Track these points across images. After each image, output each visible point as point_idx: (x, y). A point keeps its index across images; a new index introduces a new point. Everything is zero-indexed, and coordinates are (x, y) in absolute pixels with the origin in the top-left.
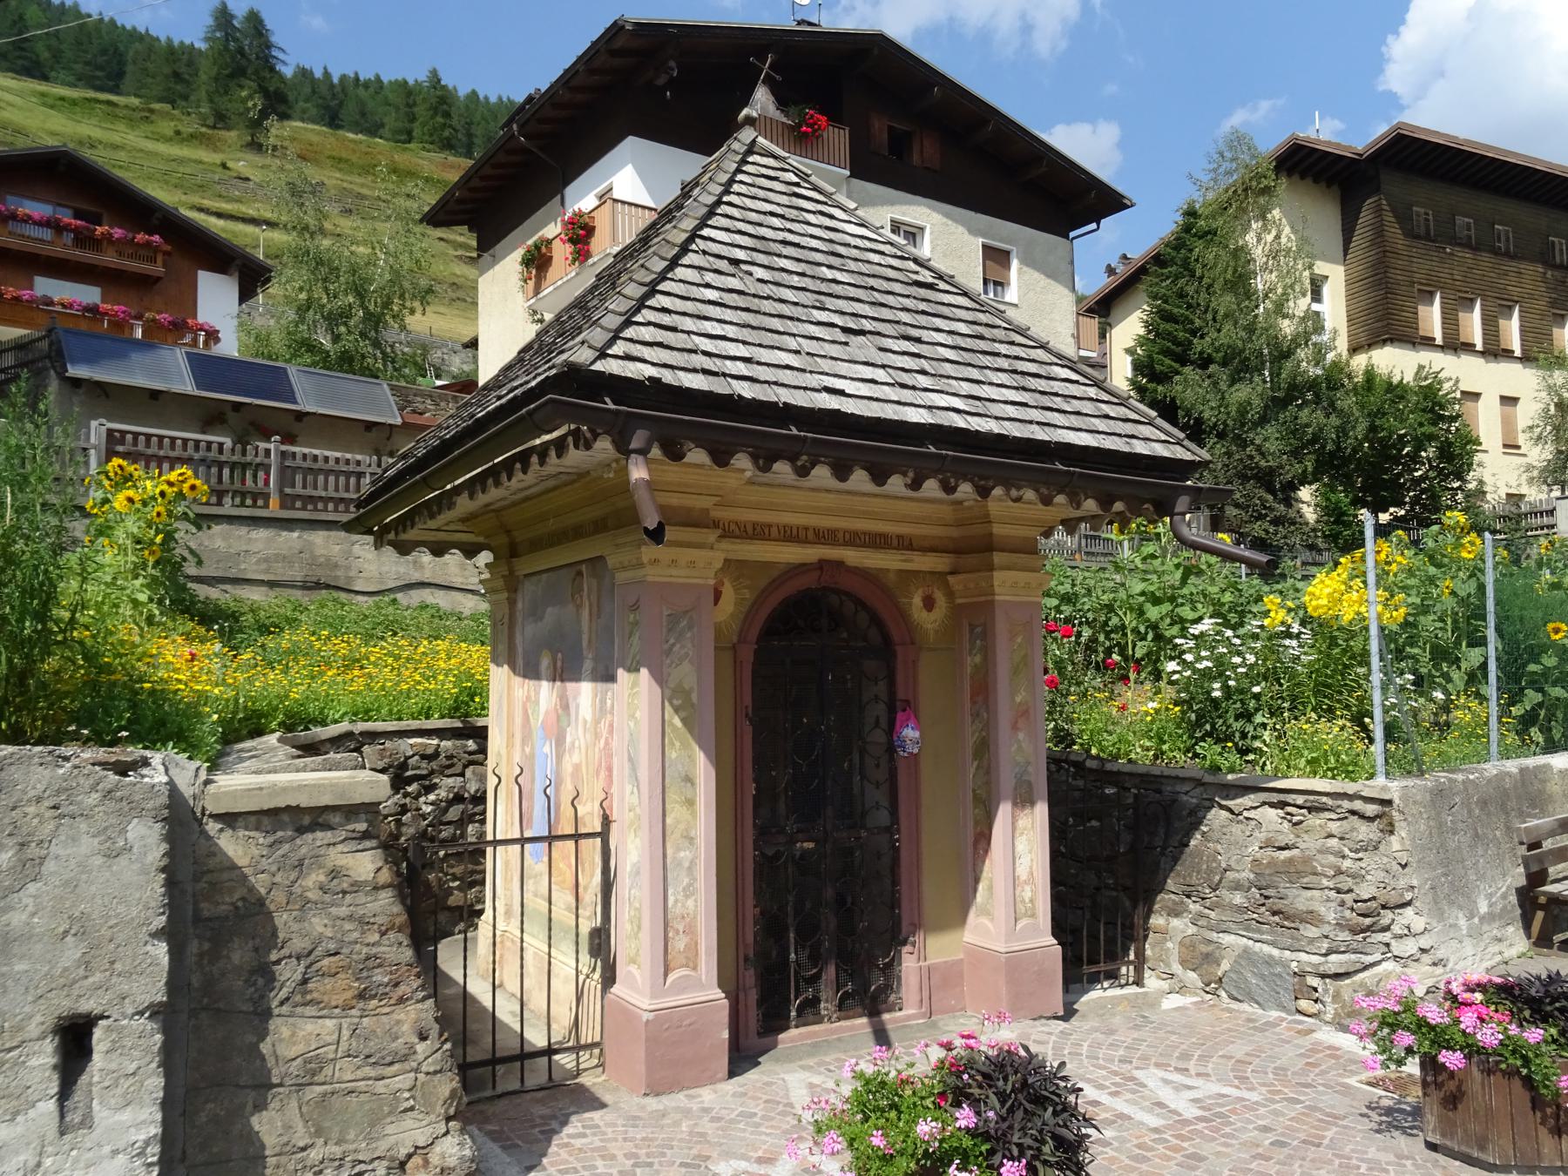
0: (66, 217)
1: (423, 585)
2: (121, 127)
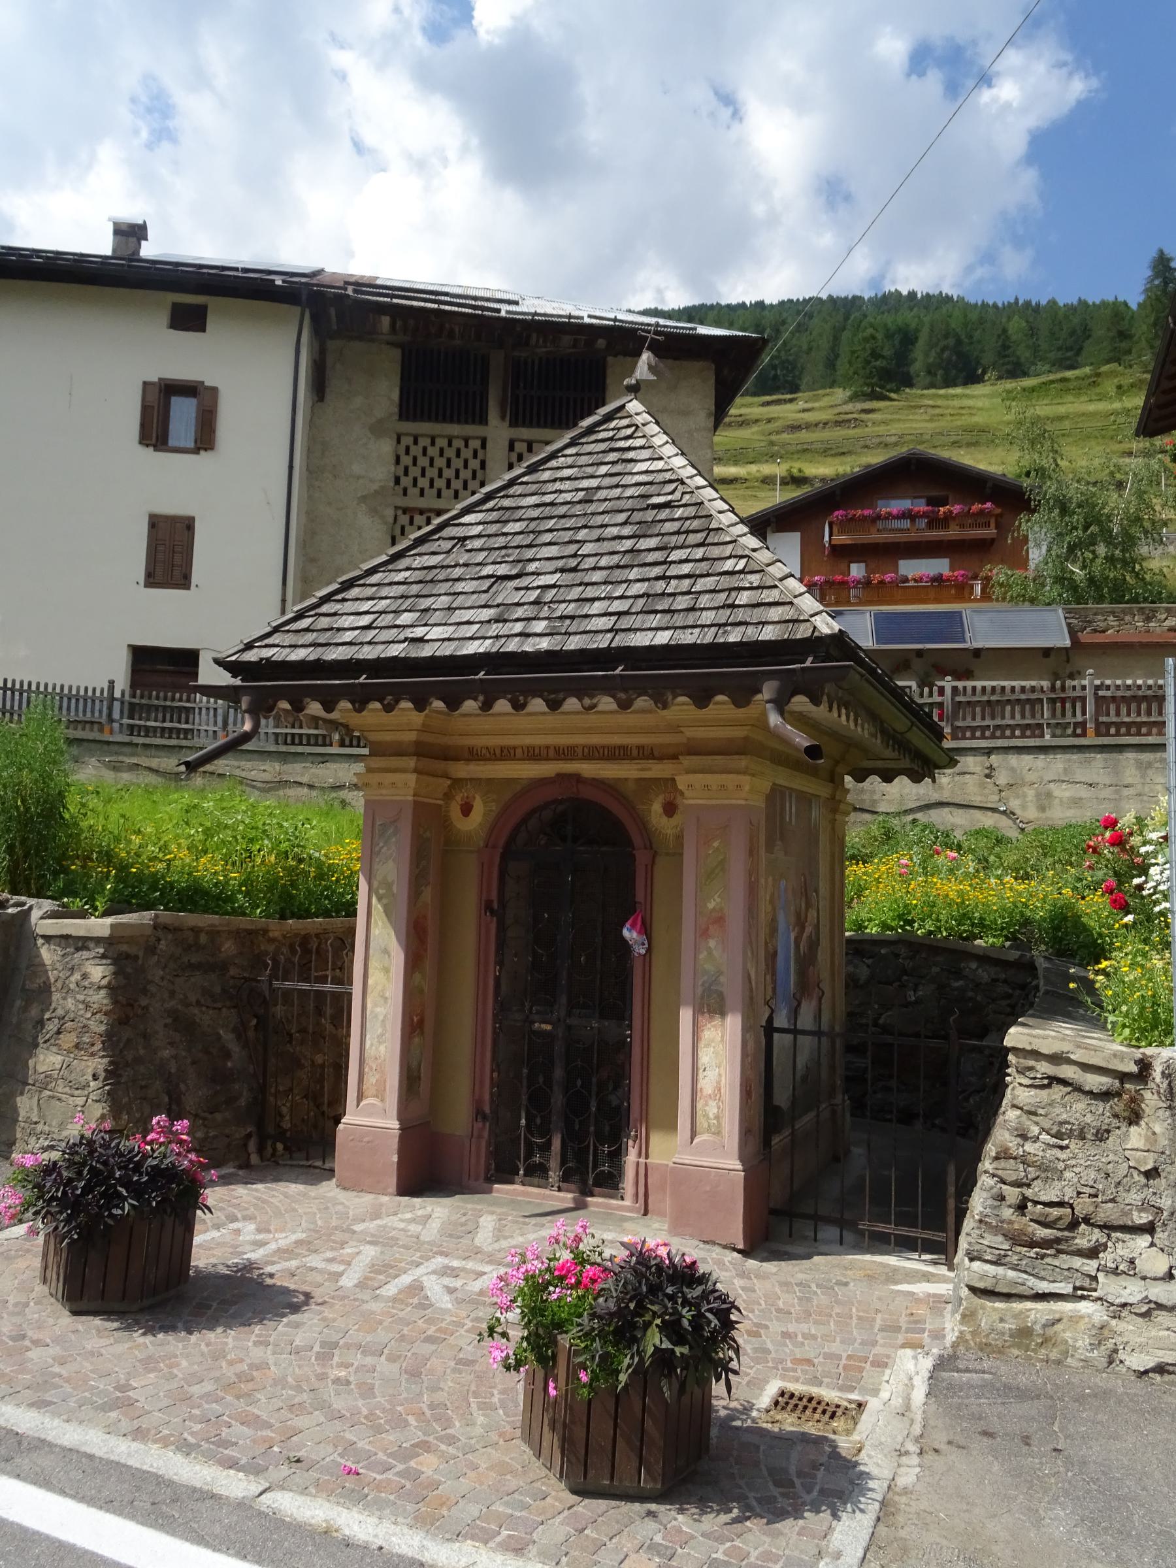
0: (921, 506)
1: (941, 804)
2: (1070, 398)
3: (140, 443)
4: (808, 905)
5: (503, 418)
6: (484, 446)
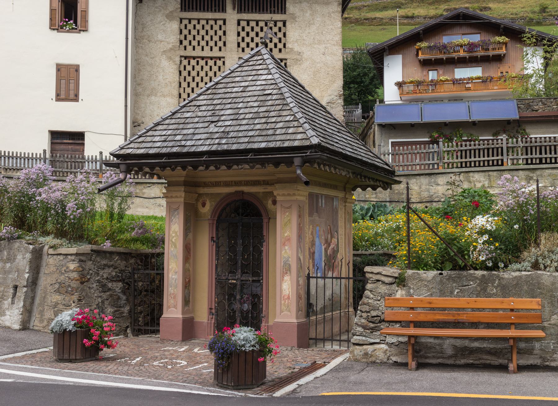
3: (50, 28)
4: (332, 237)
5: (234, 9)
6: (224, 24)
